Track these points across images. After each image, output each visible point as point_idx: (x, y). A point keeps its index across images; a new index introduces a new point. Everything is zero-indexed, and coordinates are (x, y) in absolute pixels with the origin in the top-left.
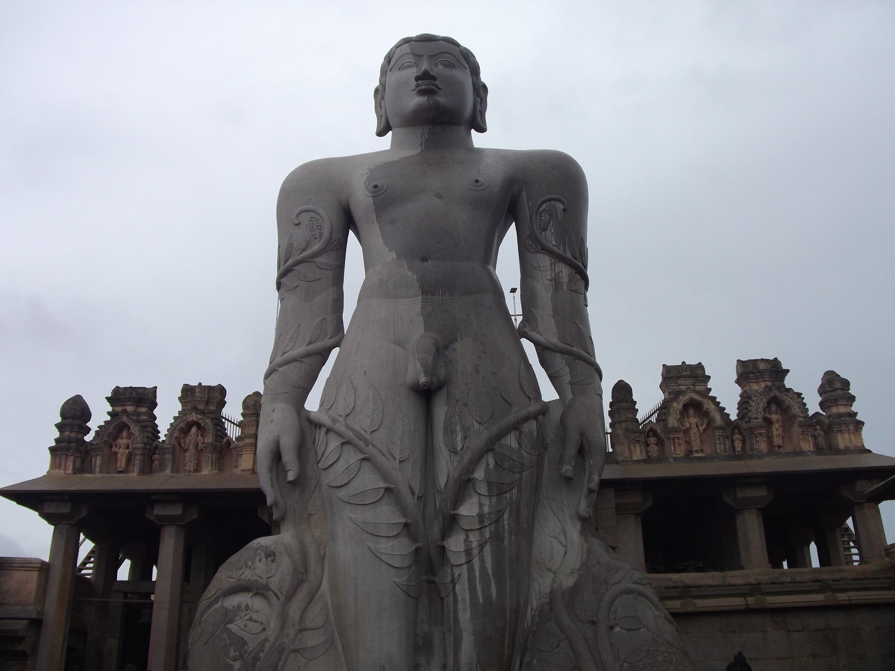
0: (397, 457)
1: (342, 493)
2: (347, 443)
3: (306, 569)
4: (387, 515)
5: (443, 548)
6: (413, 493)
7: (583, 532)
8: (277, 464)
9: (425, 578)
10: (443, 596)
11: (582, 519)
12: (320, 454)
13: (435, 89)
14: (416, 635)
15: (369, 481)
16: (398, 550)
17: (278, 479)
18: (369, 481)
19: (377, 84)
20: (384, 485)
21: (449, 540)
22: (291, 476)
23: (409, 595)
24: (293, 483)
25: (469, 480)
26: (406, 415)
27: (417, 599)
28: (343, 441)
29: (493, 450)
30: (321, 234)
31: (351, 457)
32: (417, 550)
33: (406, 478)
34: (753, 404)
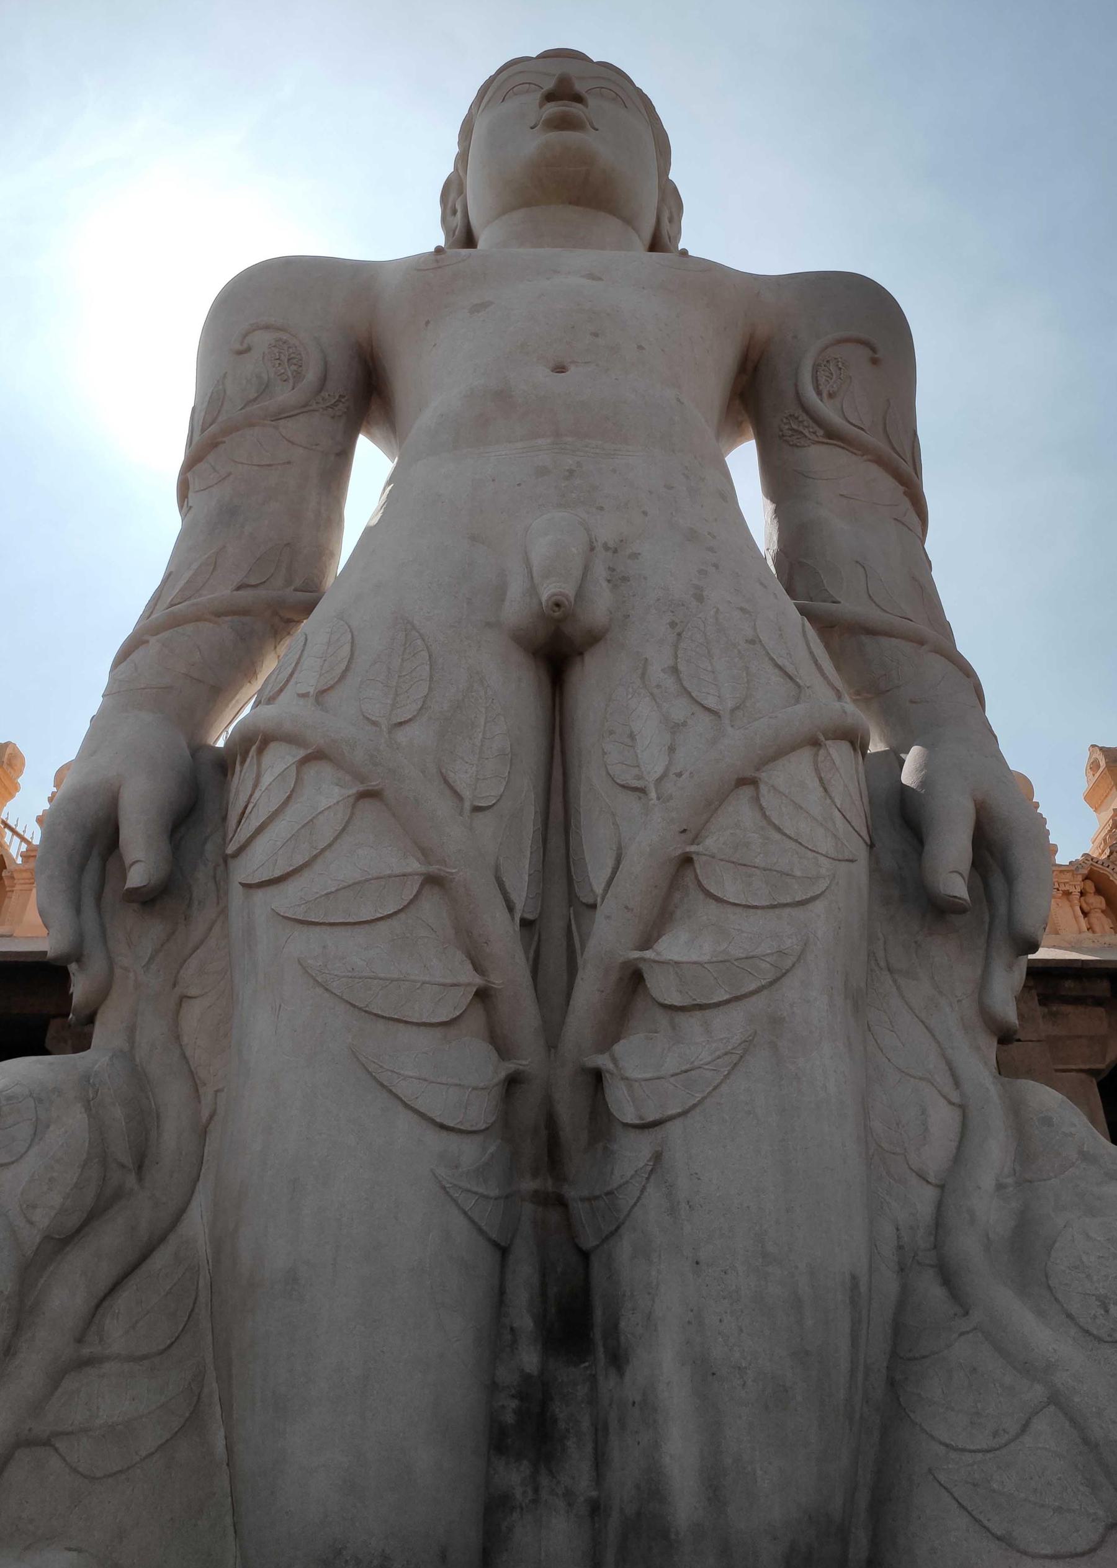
0: (467, 794)
1: (287, 898)
2: (318, 756)
3: (141, 1164)
4: (436, 975)
5: (597, 1077)
6: (511, 908)
7: (1004, 1069)
8: (104, 860)
9: (528, 1185)
10: (589, 1241)
11: (1005, 1037)
12: (230, 850)
13: (567, 145)
14: (493, 1387)
15: (372, 855)
16: (458, 1078)
17: (99, 897)
18: (372, 855)
19: (447, 168)
20: (423, 869)
21: (617, 1048)
22: (137, 877)
23: (481, 1231)
24: (149, 900)
25: (687, 860)
26: (508, 690)
27: (503, 1251)
28: (302, 753)
29: (754, 782)
30: (298, 376)
31: (327, 792)
32: (513, 1082)
33: (491, 848)
34: (1081, 1488)
